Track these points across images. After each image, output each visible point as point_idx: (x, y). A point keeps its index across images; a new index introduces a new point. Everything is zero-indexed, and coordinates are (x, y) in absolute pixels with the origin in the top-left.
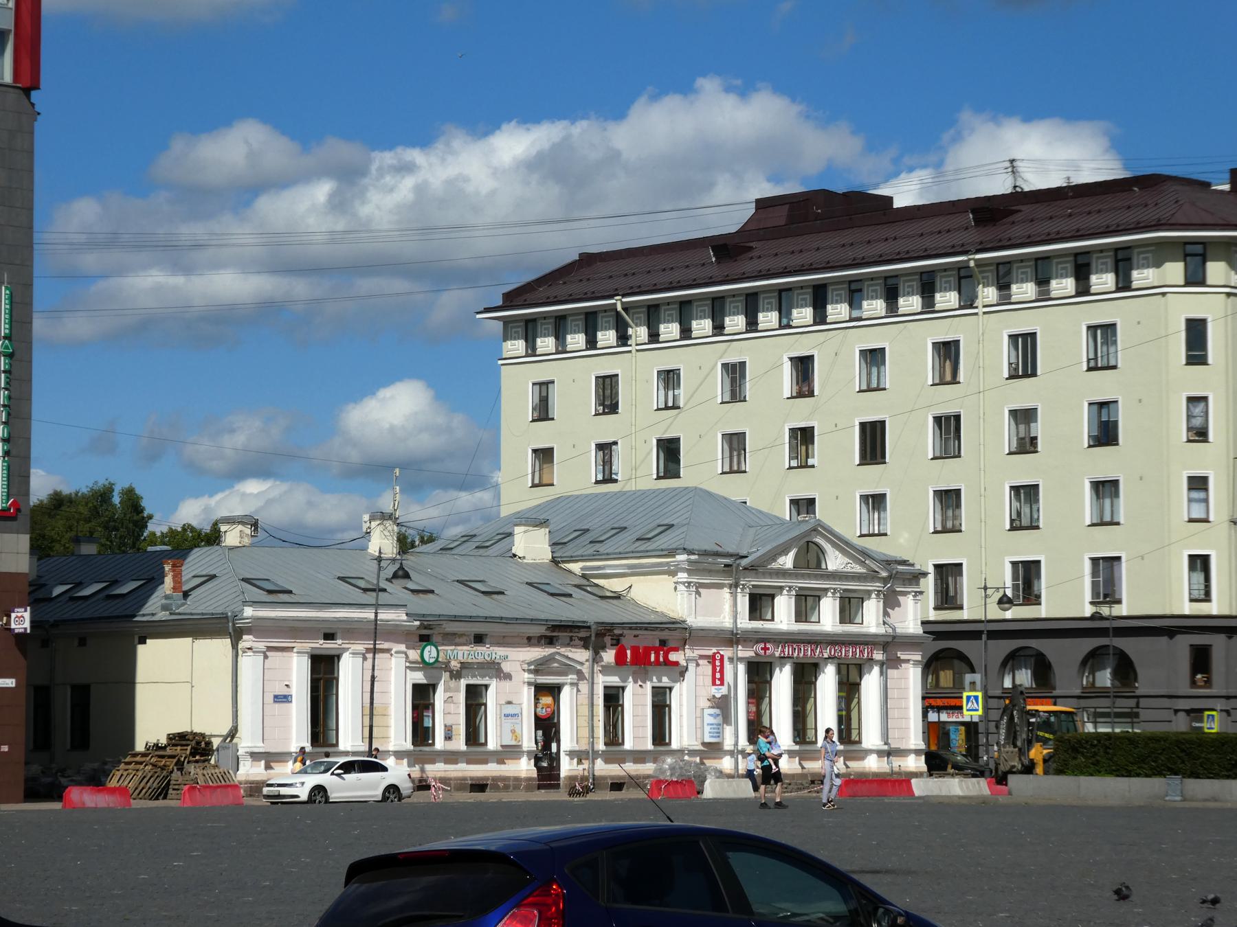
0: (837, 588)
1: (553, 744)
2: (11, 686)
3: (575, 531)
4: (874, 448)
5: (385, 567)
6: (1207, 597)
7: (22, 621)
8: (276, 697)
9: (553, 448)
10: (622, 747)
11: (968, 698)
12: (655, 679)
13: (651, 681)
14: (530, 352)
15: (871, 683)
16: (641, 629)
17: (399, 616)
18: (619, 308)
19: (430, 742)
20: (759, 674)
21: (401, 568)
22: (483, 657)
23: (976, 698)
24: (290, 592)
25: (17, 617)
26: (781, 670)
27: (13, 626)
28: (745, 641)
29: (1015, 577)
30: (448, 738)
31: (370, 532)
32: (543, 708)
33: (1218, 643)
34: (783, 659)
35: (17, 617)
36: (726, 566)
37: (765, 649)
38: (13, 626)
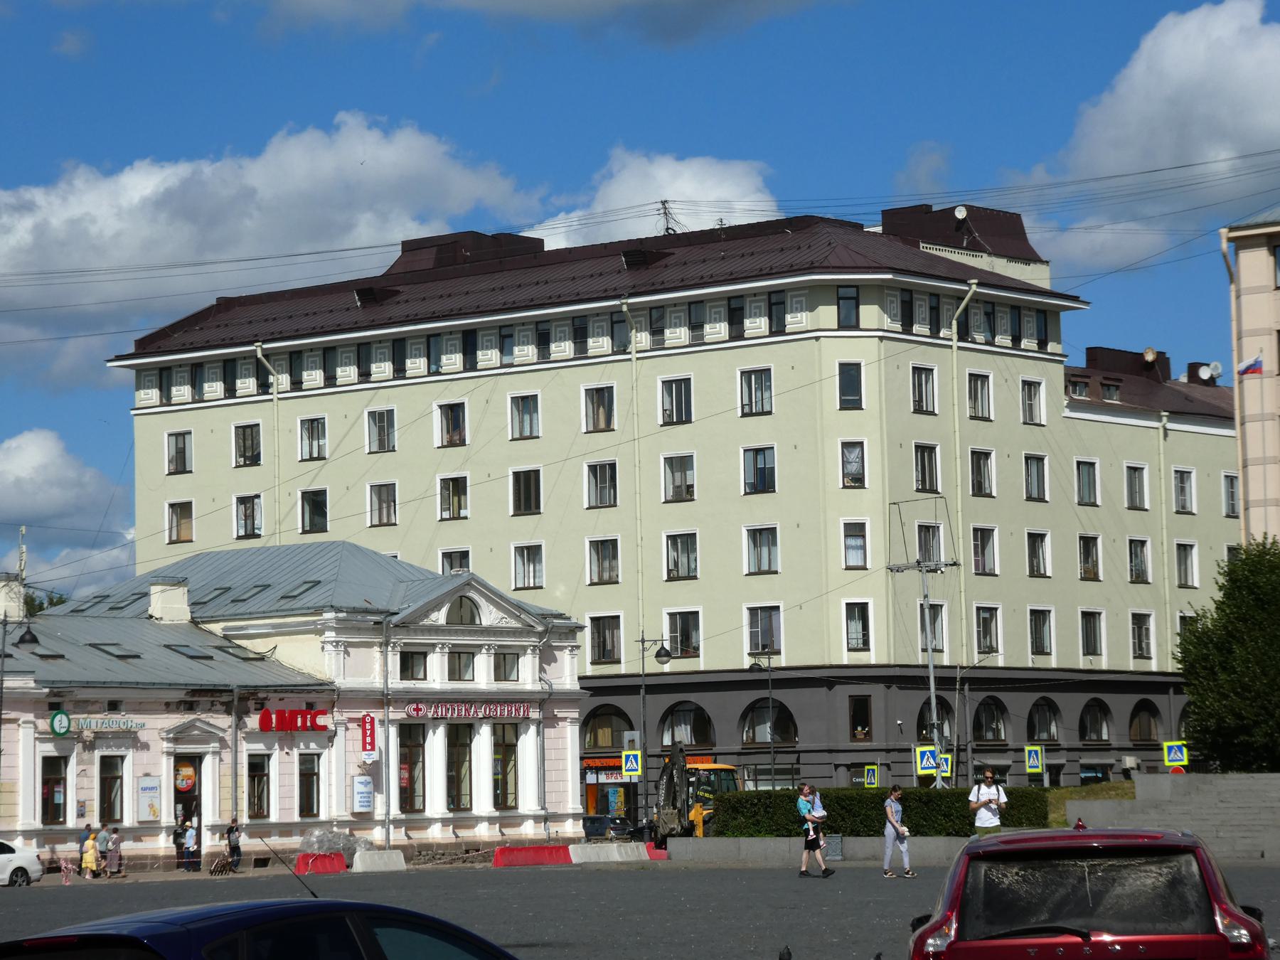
4: (528, 499)
6: (866, 647)
10: (514, 811)
11: (628, 757)
12: (302, 746)
13: (298, 747)
14: (468, 367)
15: (527, 744)
20: (412, 737)
23: (635, 757)
26: (434, 733)
28: (396, 702)
33: (876, 692)
36: (376, 623)
37: (417, 710)
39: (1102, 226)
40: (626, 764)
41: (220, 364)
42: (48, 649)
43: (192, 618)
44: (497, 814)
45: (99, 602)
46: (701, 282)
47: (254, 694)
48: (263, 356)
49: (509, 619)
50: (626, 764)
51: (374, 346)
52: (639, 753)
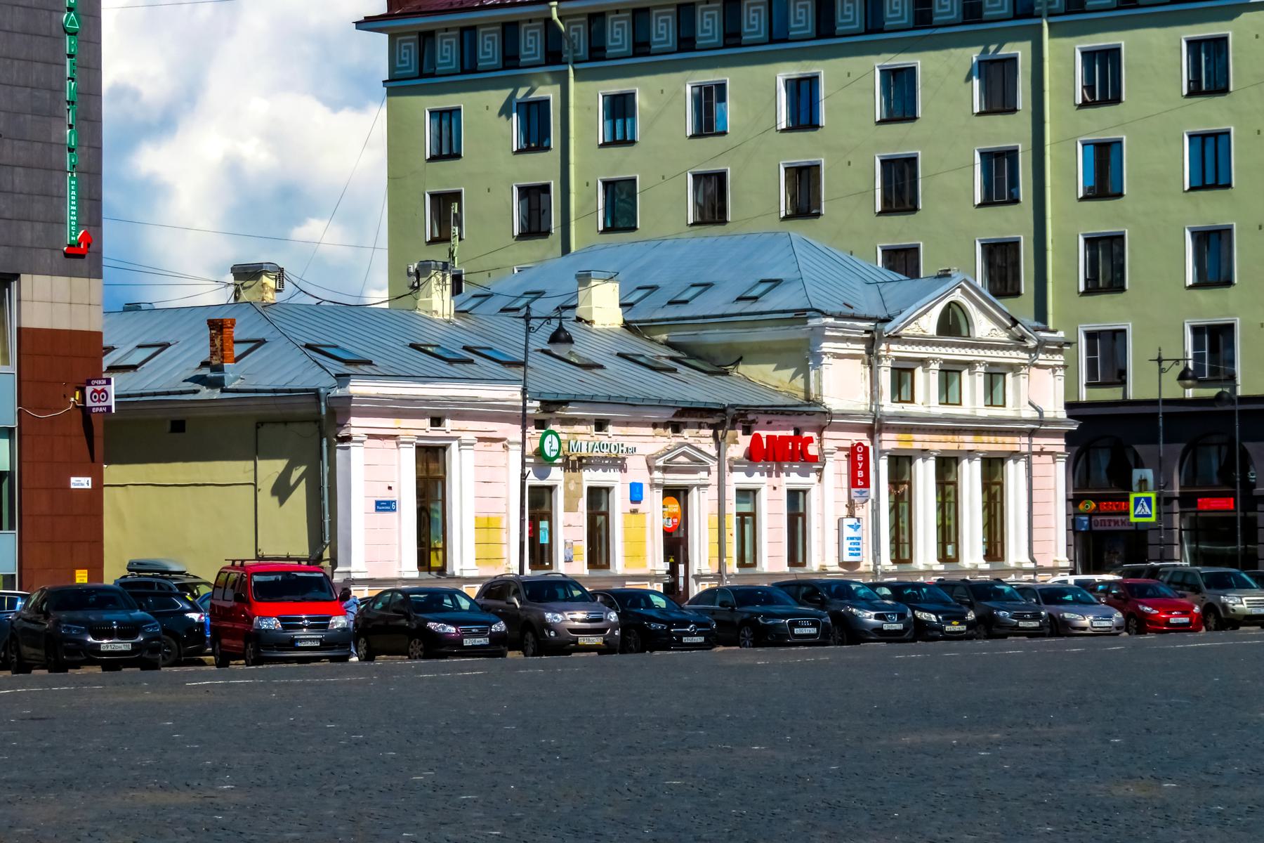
0: (982, 361)
1: (680, 565)
2: (86, 486)
3: (639, 288)
4: (900, 192)
5: (536, 328)
7: (103, 397)
8: (378, 503)
9: (818, 167)
10: (909, 564)
11: (1137, 500)
14: (550, 60)
16: (777, 414)
17: (513, 395)
18: (555, 16)
19: (547, 564)
21: (561, 329)
22: (608, 450)
23: (1148, 500)
24: (369, 363)
25: (95, 391)
27: (89, 403)
29: (1197, 345)
30: (569, 560)
31: (418, 288)
32: (669, 518)
34: (924, 453)
35: (95, 391)
38: (89, 403)
39: (1120, 633)
40: (1135, 508)
41: (415, 37)
42: (147, 367)
43: (625, 322)
44: (987, 566)
45: (536, 298)
46: (450, 8)
47: (744, 415)
48: (560, 18)
49: (998, 331)
50: (1135, 508)
51: (524, 26)
52: (1153, 496)
